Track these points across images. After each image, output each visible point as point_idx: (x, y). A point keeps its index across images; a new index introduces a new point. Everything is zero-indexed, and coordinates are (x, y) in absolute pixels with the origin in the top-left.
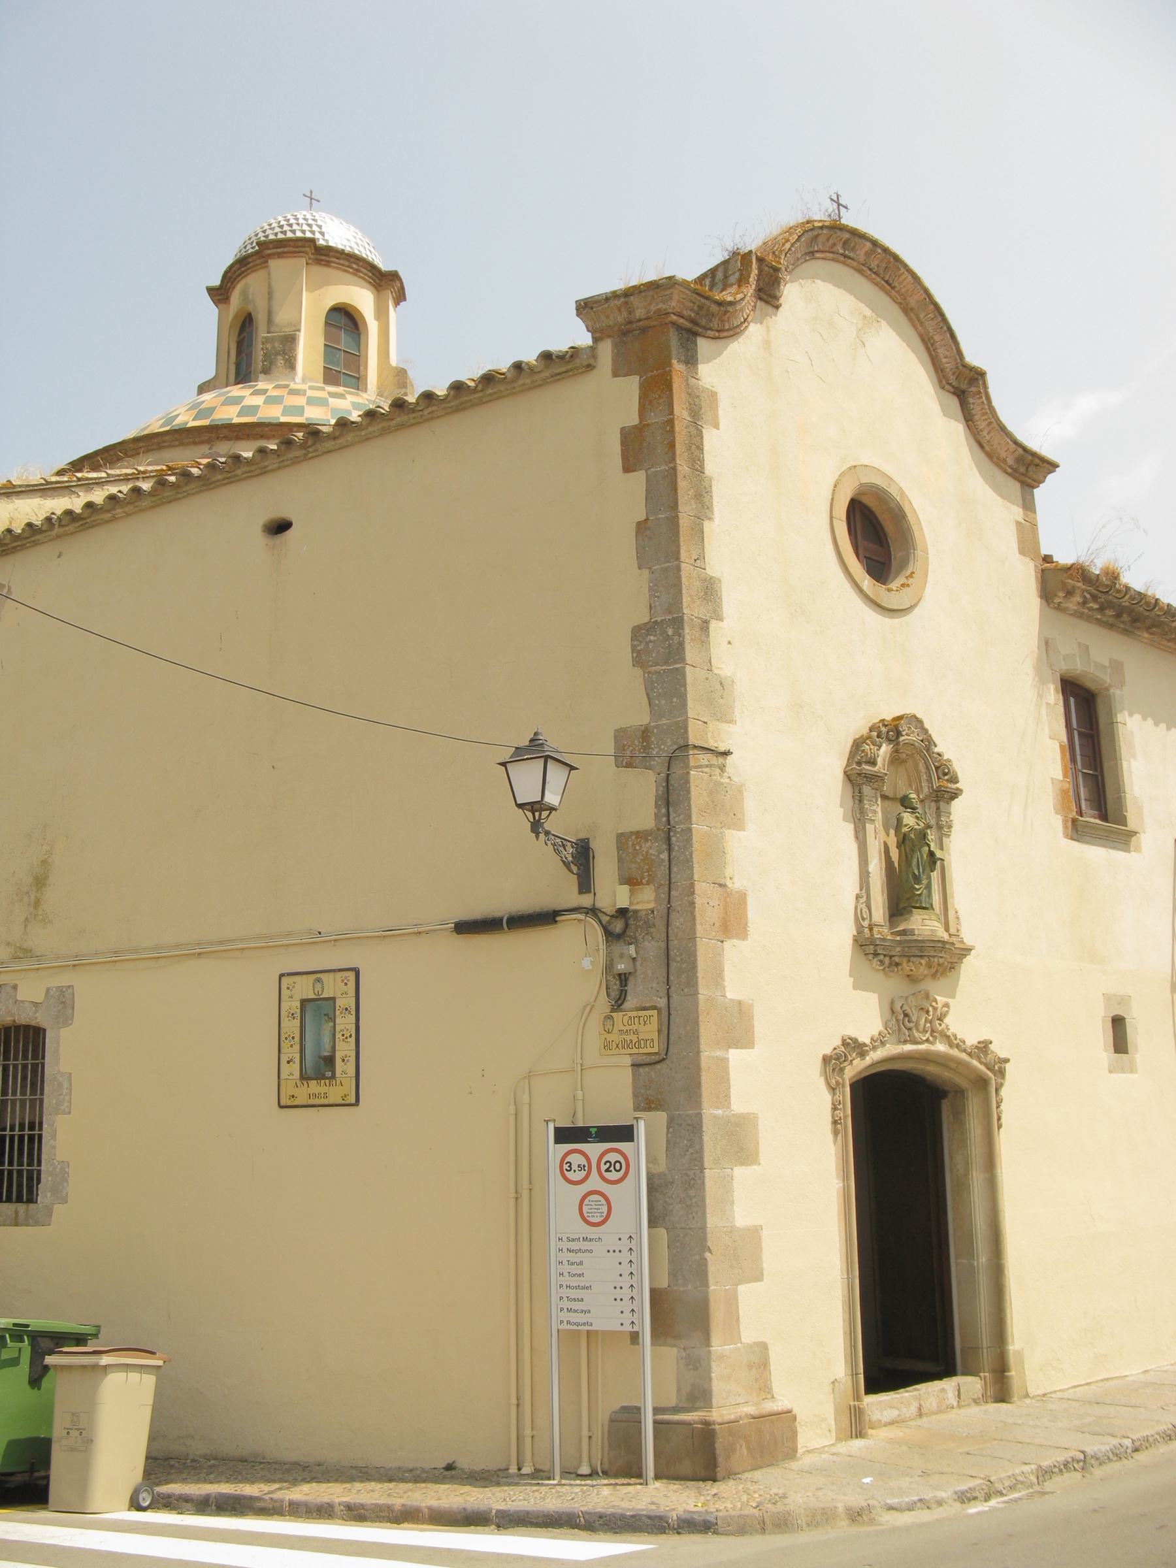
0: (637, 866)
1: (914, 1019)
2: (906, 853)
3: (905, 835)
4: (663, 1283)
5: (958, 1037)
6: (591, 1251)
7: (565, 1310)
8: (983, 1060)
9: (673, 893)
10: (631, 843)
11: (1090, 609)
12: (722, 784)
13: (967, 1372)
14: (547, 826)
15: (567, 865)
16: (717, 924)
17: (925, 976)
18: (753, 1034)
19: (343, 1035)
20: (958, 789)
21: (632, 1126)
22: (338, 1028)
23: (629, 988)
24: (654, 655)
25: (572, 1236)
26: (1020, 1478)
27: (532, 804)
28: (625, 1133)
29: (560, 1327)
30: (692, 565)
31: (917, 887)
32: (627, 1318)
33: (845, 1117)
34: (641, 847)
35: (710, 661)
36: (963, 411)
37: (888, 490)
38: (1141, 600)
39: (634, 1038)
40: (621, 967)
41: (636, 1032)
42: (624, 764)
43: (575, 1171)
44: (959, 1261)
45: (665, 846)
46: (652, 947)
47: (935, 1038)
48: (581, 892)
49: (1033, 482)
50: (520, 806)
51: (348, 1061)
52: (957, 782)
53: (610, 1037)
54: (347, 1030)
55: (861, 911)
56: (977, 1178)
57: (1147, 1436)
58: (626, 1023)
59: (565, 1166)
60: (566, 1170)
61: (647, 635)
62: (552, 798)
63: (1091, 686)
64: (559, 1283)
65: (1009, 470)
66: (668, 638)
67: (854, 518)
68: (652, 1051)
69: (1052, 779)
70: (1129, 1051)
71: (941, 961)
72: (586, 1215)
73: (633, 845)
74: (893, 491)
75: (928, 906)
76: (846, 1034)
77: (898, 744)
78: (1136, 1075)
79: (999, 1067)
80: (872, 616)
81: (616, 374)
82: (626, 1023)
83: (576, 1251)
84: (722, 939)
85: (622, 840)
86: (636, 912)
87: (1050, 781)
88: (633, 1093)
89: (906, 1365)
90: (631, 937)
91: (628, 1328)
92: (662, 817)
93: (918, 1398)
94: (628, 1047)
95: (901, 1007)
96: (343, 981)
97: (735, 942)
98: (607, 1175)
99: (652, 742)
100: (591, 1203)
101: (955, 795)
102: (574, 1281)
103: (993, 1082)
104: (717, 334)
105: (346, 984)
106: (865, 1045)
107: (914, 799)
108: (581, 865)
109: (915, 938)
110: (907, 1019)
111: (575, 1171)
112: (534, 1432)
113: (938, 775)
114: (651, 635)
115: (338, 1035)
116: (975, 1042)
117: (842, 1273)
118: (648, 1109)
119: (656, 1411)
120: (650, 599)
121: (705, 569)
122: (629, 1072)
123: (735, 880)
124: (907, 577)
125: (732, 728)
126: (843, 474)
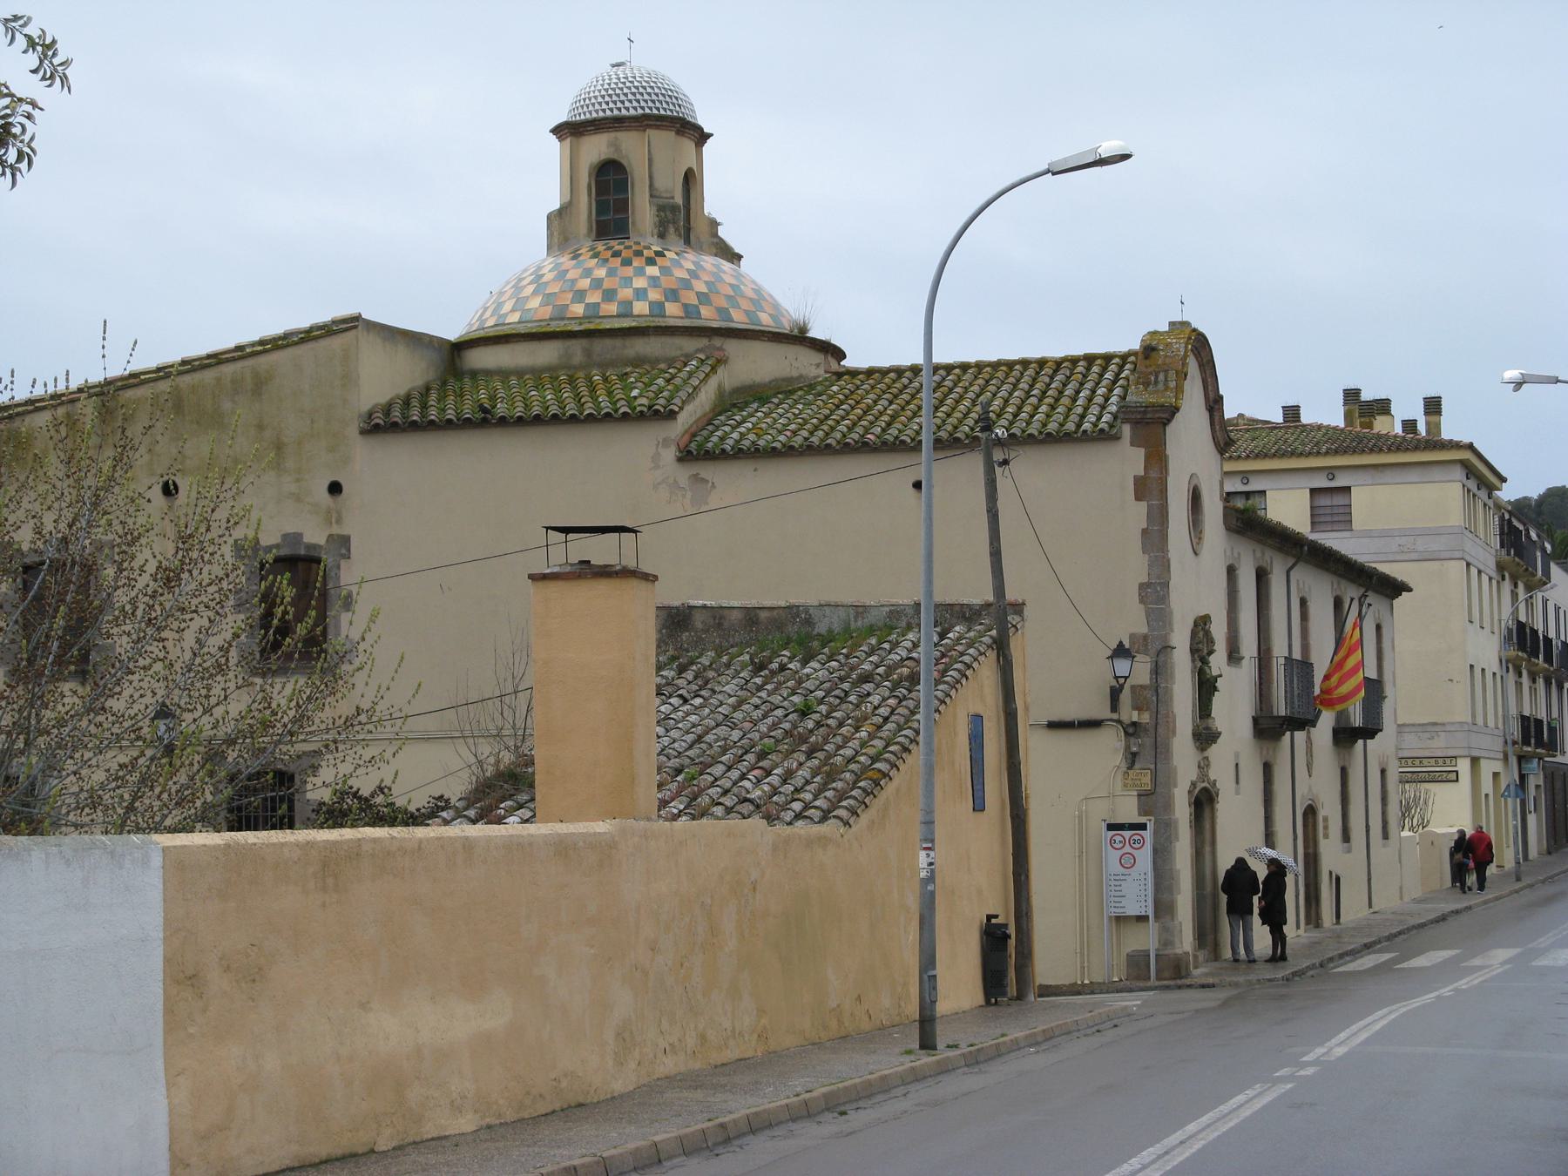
23: (1137, 760)
28: (1143, 827)
46: (1148, 741)
66: (1158, 592)
81: (1132, 445)
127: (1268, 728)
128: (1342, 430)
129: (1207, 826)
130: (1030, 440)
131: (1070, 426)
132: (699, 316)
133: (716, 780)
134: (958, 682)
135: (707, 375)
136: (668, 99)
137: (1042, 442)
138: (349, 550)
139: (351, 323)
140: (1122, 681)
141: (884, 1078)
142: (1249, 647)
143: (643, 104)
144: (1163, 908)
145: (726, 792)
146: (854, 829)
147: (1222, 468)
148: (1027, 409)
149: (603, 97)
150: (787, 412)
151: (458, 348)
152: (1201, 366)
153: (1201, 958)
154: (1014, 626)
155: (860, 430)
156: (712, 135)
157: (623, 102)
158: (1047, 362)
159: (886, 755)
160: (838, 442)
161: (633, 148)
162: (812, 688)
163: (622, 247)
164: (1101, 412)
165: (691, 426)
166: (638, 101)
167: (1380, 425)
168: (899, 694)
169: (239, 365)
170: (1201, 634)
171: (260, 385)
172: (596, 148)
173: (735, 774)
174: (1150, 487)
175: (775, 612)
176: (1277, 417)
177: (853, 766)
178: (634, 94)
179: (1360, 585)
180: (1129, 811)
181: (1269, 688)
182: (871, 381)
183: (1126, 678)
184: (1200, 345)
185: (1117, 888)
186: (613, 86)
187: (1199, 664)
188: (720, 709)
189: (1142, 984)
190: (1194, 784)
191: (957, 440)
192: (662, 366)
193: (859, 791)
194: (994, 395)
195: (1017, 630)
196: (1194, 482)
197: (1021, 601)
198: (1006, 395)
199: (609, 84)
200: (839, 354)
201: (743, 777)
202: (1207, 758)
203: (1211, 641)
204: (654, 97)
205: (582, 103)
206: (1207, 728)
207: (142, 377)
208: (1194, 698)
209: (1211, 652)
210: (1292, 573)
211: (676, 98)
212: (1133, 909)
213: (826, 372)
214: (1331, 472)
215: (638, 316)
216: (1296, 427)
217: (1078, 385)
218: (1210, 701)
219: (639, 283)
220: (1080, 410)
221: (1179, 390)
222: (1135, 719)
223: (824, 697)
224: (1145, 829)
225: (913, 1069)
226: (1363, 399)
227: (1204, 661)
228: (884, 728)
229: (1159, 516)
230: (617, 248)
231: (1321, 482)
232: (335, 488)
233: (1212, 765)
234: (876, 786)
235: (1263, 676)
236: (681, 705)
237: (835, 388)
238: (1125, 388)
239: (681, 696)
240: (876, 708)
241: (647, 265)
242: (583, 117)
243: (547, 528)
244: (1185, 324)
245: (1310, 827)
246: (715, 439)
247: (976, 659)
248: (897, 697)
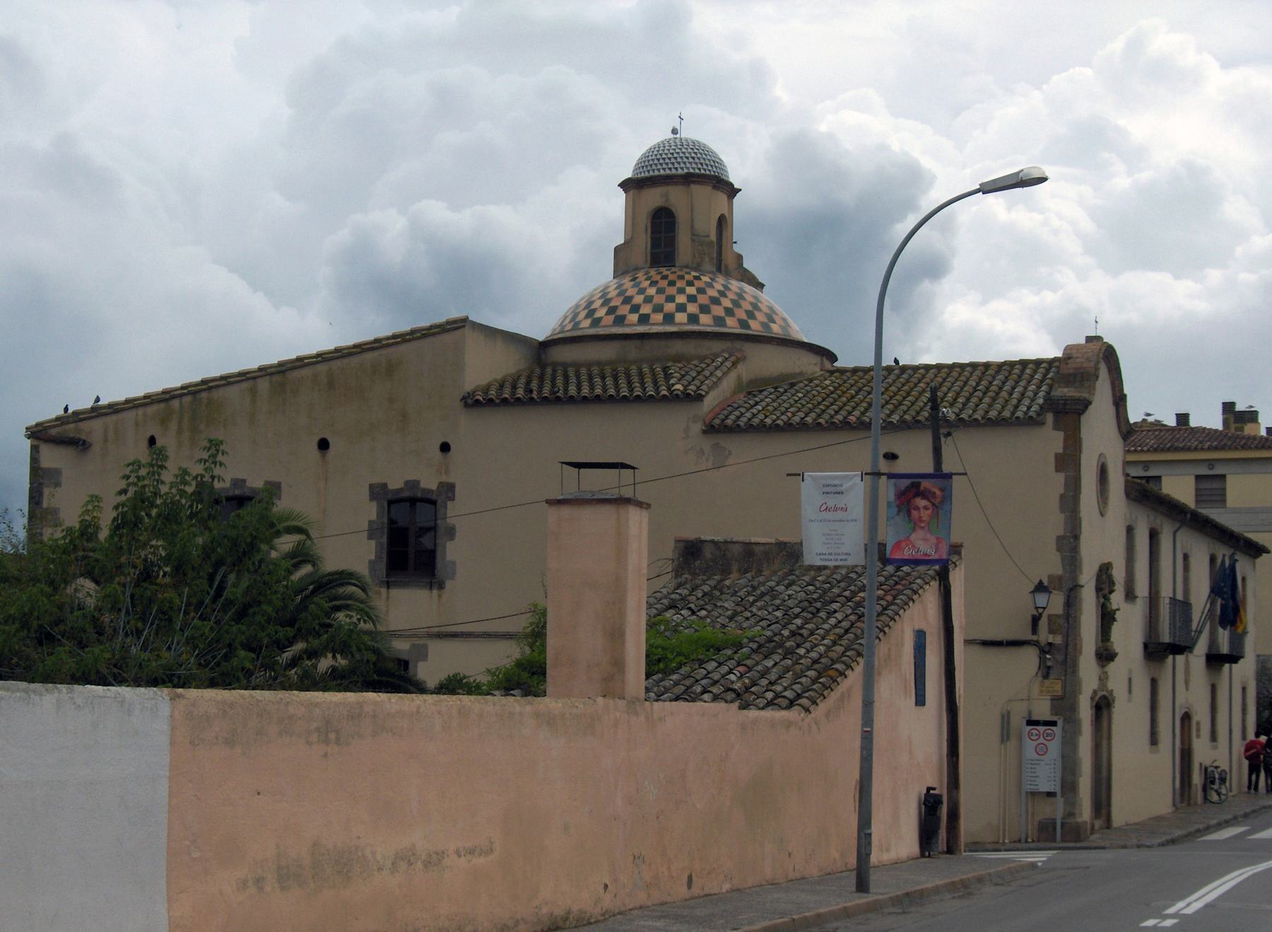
23: (1051, 672)
66: (1071, 542)
86: (1055, 644)
93: (203, 692)
98: (1047, 738)
104: (411, 337)
127: (1156, 651)
128: (1221, 431)
129: (1105, 724)
130: (974, 423)
131: (1006, 414)
132: (724, 325)
133: (709, 673)
134: (906, 604)
135: (729, 369)
136: (707, 162)
137: (984, 425)
138: (454, 495)
139: (461, 324)
140: (1041, 610)
141: (819, 916)
142: (1142, 588)
143: (688, 165)
144: (1069, 786)
145: (715, 683)
146: (813, 715)
147: (1125, 458)
148: (974, 400)
149: (658, 160)
150: (789, 398)
151: (546, 345)
152: (1110, 371)
153: (1097, 827)
154: (954, 563)
155: (843, 413)
156: (740, 190)
157: (673, 164)
158: (991, 365)
159: (844, 658)
160: (827, 422)
161: (676, 197)
162: (792, 606)
163: (668, 273)
164: (1030, 403)
165: (715, 407)
166: (685, 163)
167: (1248, 429)
168: (859, 612)
169: (376, 354)
170: (1104, 577)
171: (391, 369)
172: (654, 198)
173: (724, 669)
174: (1068, 461)
175: (767, 547)
176: (1171, 422)
177: (816, 666)
178: (681, 158)
179: (1231, 547)
180: (1043, 710)
181: (1157, 621)
182: (856, 378)
183: (1044, 608)
184: (1109, 355)
185: (1033, 770)
186: (666, 151)
187: (1102, 600)
188: (718, 620)
189: (1048, 845)
190: (1095, 692)
191: (919, 422)
192: (695, 362)
193: (820, 685)
194: (950, 389)
195: (956, 566)
196: (1103, 460)
197: (959, 544)
198: (958, 389)
199: (663, 150)
200: (832, 357)
201: (730, 672)
202: (1106, 673)
203: (1112, 583)
204: (697, 160)
205: (647, 163)
206: (1106, 650)
207: (306, 361)
208: (1097, 627)
209: (1111, 592)
210: (1178, 534)
211: (714, 162)
212: (1045, 787)
213: (821, 370)
214: (1211, 463)
215: (679, 324)
216: (1186, 429)
217: (1014, 383)
218: (1110, 628)
219: (681, 299)
220: (1014, 402)
221: (1092, 389)
222: (1050, 640)
223: (800, 613)
225: (845, 908)
226: (1237, 410)
227: (1106, 598)
228: (845, 637)
229: (1074, 485)
230: (666, 273)
231: (1204, 471)
232: (445, 448)
233: (1110, 678)
234: (833, 682)
235: (1153, 616)
236: (689, 616)
237: (827, 382)
238: (1051, 387)
239: (690, 609)
240: (840, 622)
241: (688, 286)
242: (643, 175)
243: (562, 463)
244: (1099, 338)
245: (1186, 729)
246: (732, 417)
247: (921, 587)
248: (856, 614)
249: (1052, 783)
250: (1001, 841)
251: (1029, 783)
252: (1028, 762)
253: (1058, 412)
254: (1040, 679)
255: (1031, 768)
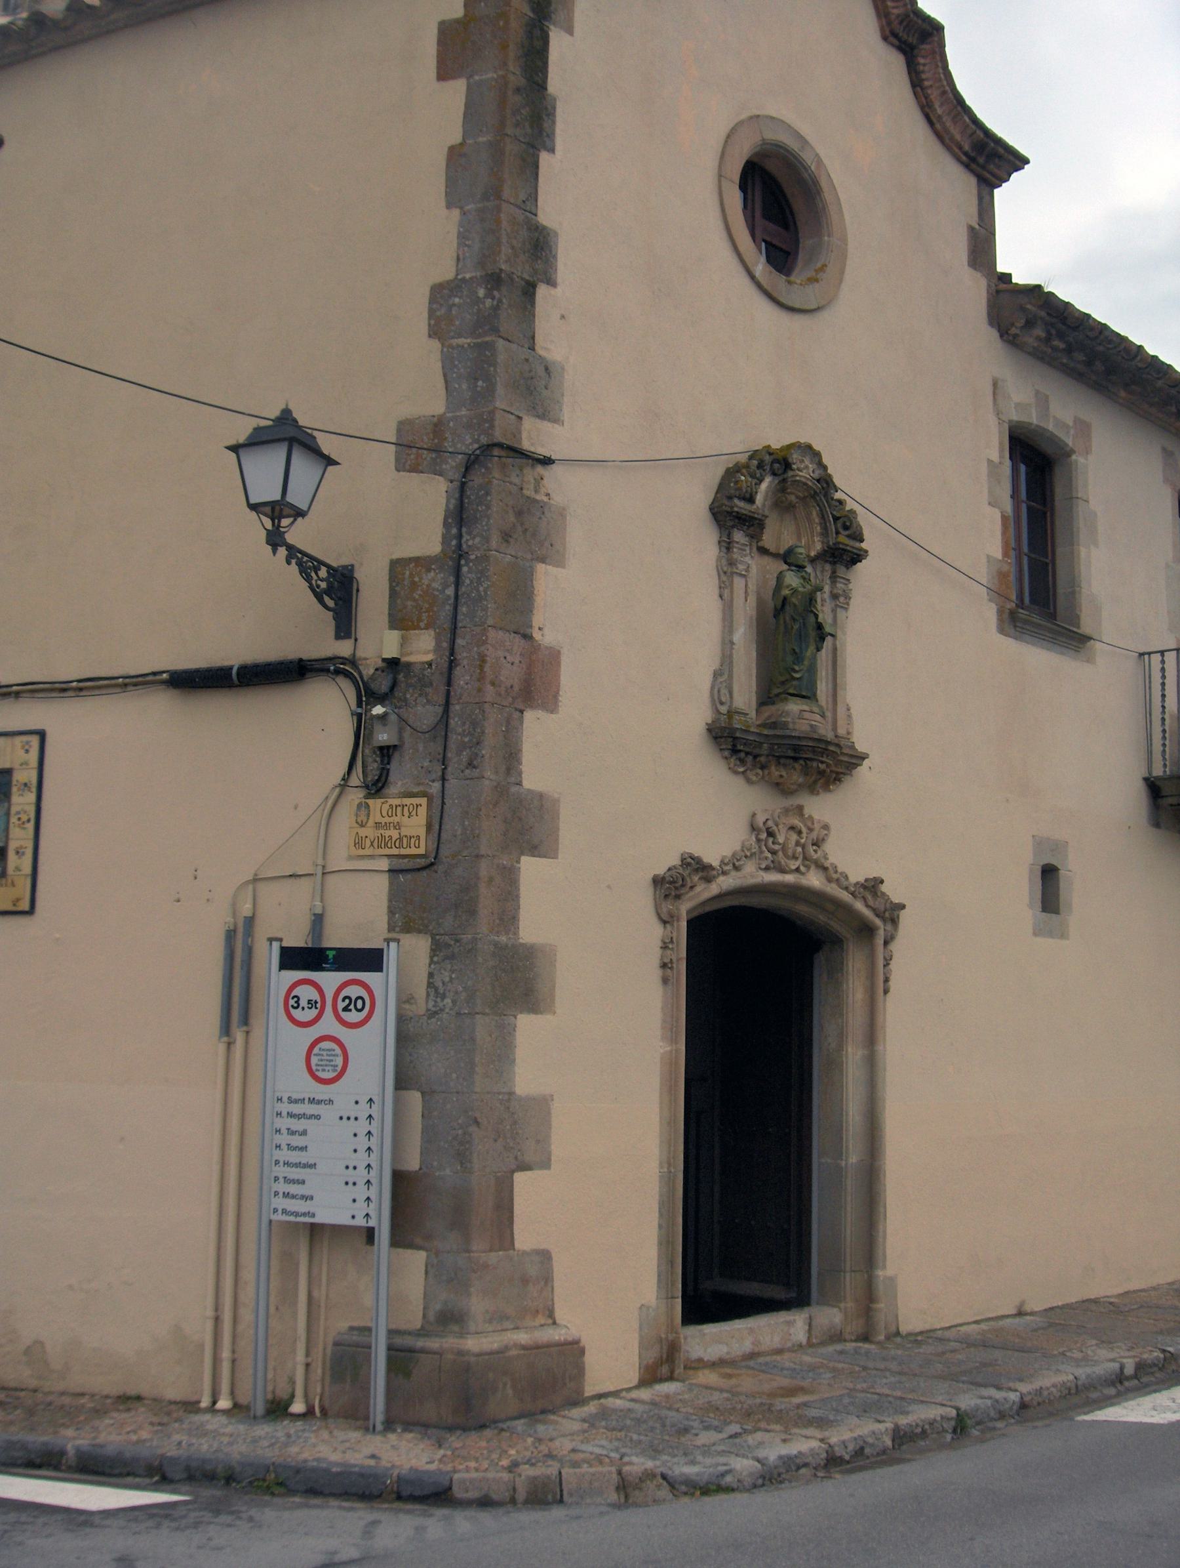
0: (414, 604)
1: (781, 839)
2: (785, 622)
3: (785, 599)
4: (413, 1163)
5: (840, 870)
6: (318, 1117)
7: (281, 1195)
8: (871, 903)
9: (460, 642)
10: (408, 573)
11: (1055, 349)
12: (535, 501)
13: (824, 1302)
14: (290, 538)
15: (319, 597)
16: (516, 688)
17: (800, 785)
18: (557, 840)
19: (19, 819)
20: (861, 549)
21: (382, 950)
22: (14, 810)
23: (394, 766)
24: (457, 323)
25: (295, 1096)
26: (870, 1440)
27: (272, 504)
28: (371, 960)
29: (274, 1217)
30: (519, 208)
31: (797, 668)
32: (361, 1209)
33: (678, 960)
34: (421, 579)
35: (533, 338)
36: (909, 73)
37: (801, 154)
38: (1120, 344)
39: (395, 834)
40: (383, 737)
41: (398, 826)
42: (407, 467)
43: (303, 1008)
44: (823, 1160)
45: (452, 579)
47: (808, 868)
48: (338, 637)
49: (993, 179)
50: (254, 507)
51: (23, 853)
52: (862, 541)
53: (363, 832)
54: (25, 812)
55: (719, 691)
56: (853, 1055)
57: (1041, 1388)
58: (384, 814)
59: (291, 1002)
60: (292, 1006)
61: (450, 297)
62: (297, 498)
63: (1049, 450)
64: (275, 1158)
65: (964, 158)
66: (478, 301)
67: (753, 195)
68: (414, 851)
69: (988, 556)
70: (1061, 912)
71: (822, 766)
72: (314, 1068)
73: (411, 575)
74: (807, 157)
75: (809, 695)
76: (687, 851)
77: (784, 480)
78: (1068, 942)
79: (892, 913)
80: (764, 310)
82: (384, 814)
83: (299, 1117)
84: (523, 708)
85: (396, 566)
87: (984, 560)
88: (389, 907)
89: (754, 1289)
90: (400, 699)
91: (360, 1222)
92: (451, 541)
94: (386, 845)
95: (764, 823)
96: (23, 747)
97: (540, 713)
98: (344, 1015)
99: (446, 438)
100: (322, 1052)
101: (856, 557)
102: (294, 1157)
103: (881, 932)
105: (27, 751)
106: (711, 867)
107: (801, 554)
108: (340, 599)
109: (788, 733)
110: (771, 840)
111: (303, 1008)
112: (236, 1356)
113: (836, 529)
114: (456, 296)
115: (13, 820)
116: (861, 879)
117: (661, 1164)
118: (407, 929)
119: (391, 1333)
120: (458, 249)
121: (536, 215)
122: (383, 882)
123: (546, 630)
124: (816, 271)
125: (556, 429)
126: (741, 123)
185: (297, 1141)
224: (379, 968)
249: (361, 1192)
250: (205, 1403)
251: (282, 1187)
252: (280, 1107)
253: (1085, 501)
254: (355, 796)
255: (292, 1132)
